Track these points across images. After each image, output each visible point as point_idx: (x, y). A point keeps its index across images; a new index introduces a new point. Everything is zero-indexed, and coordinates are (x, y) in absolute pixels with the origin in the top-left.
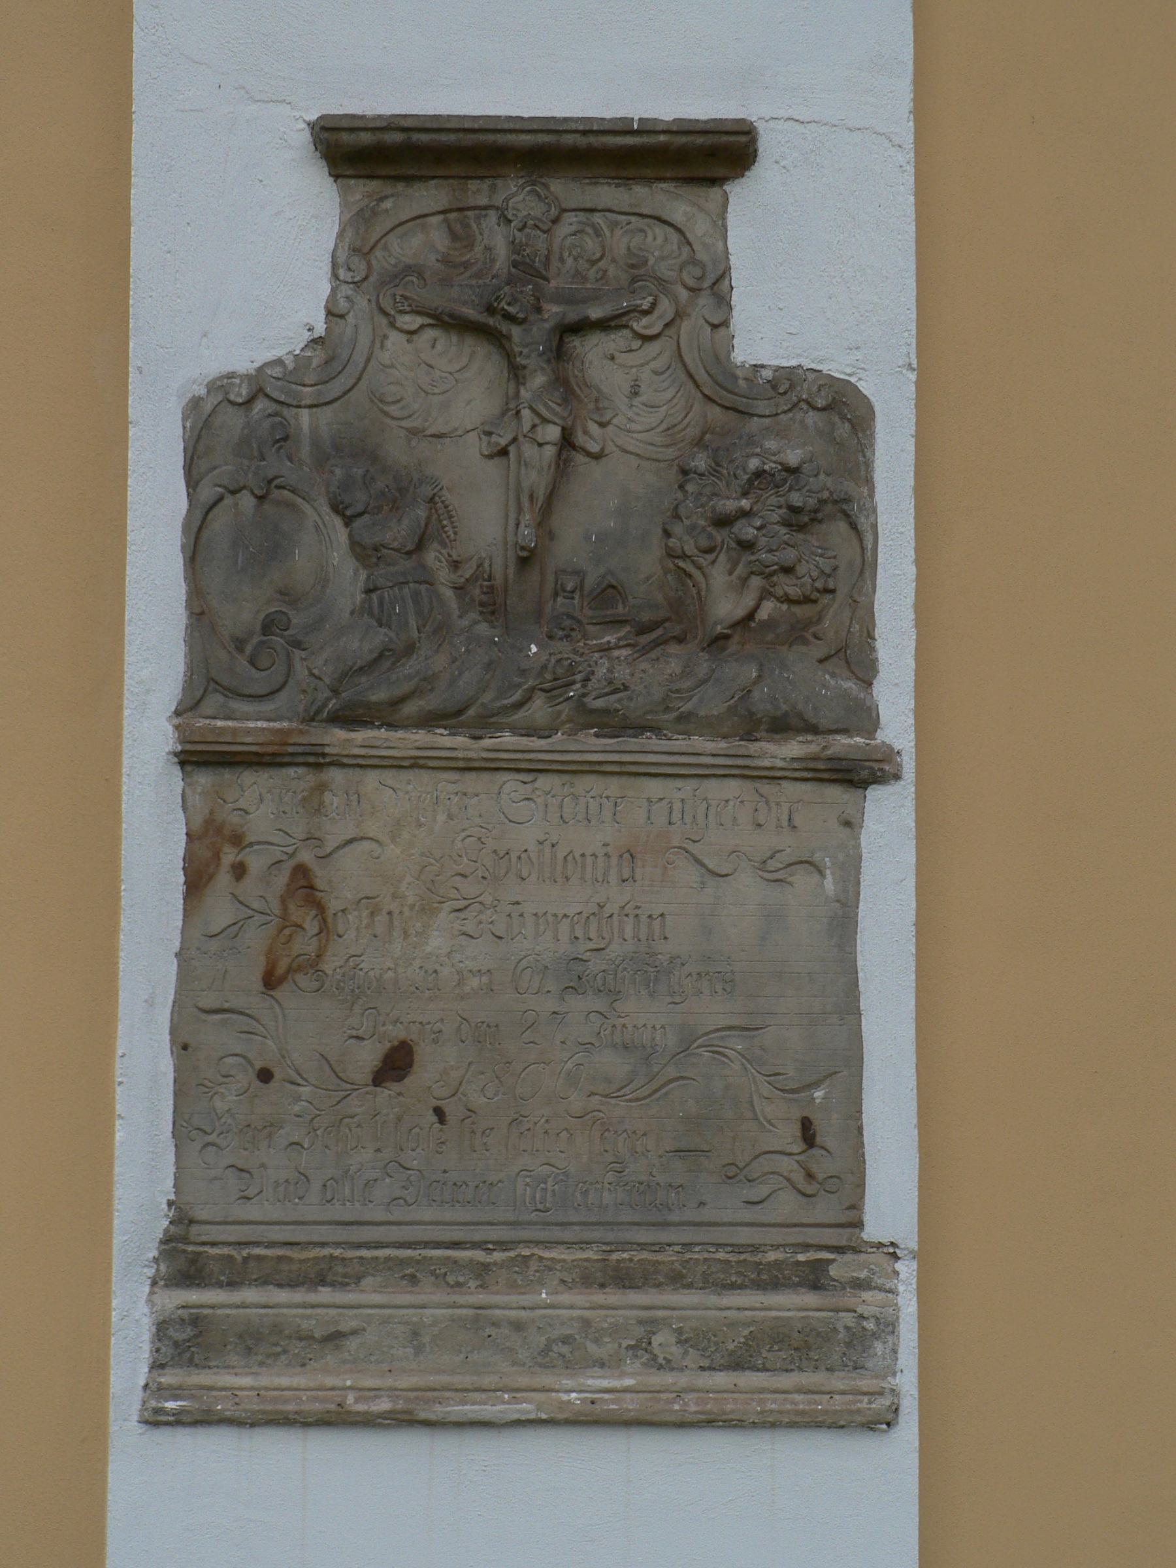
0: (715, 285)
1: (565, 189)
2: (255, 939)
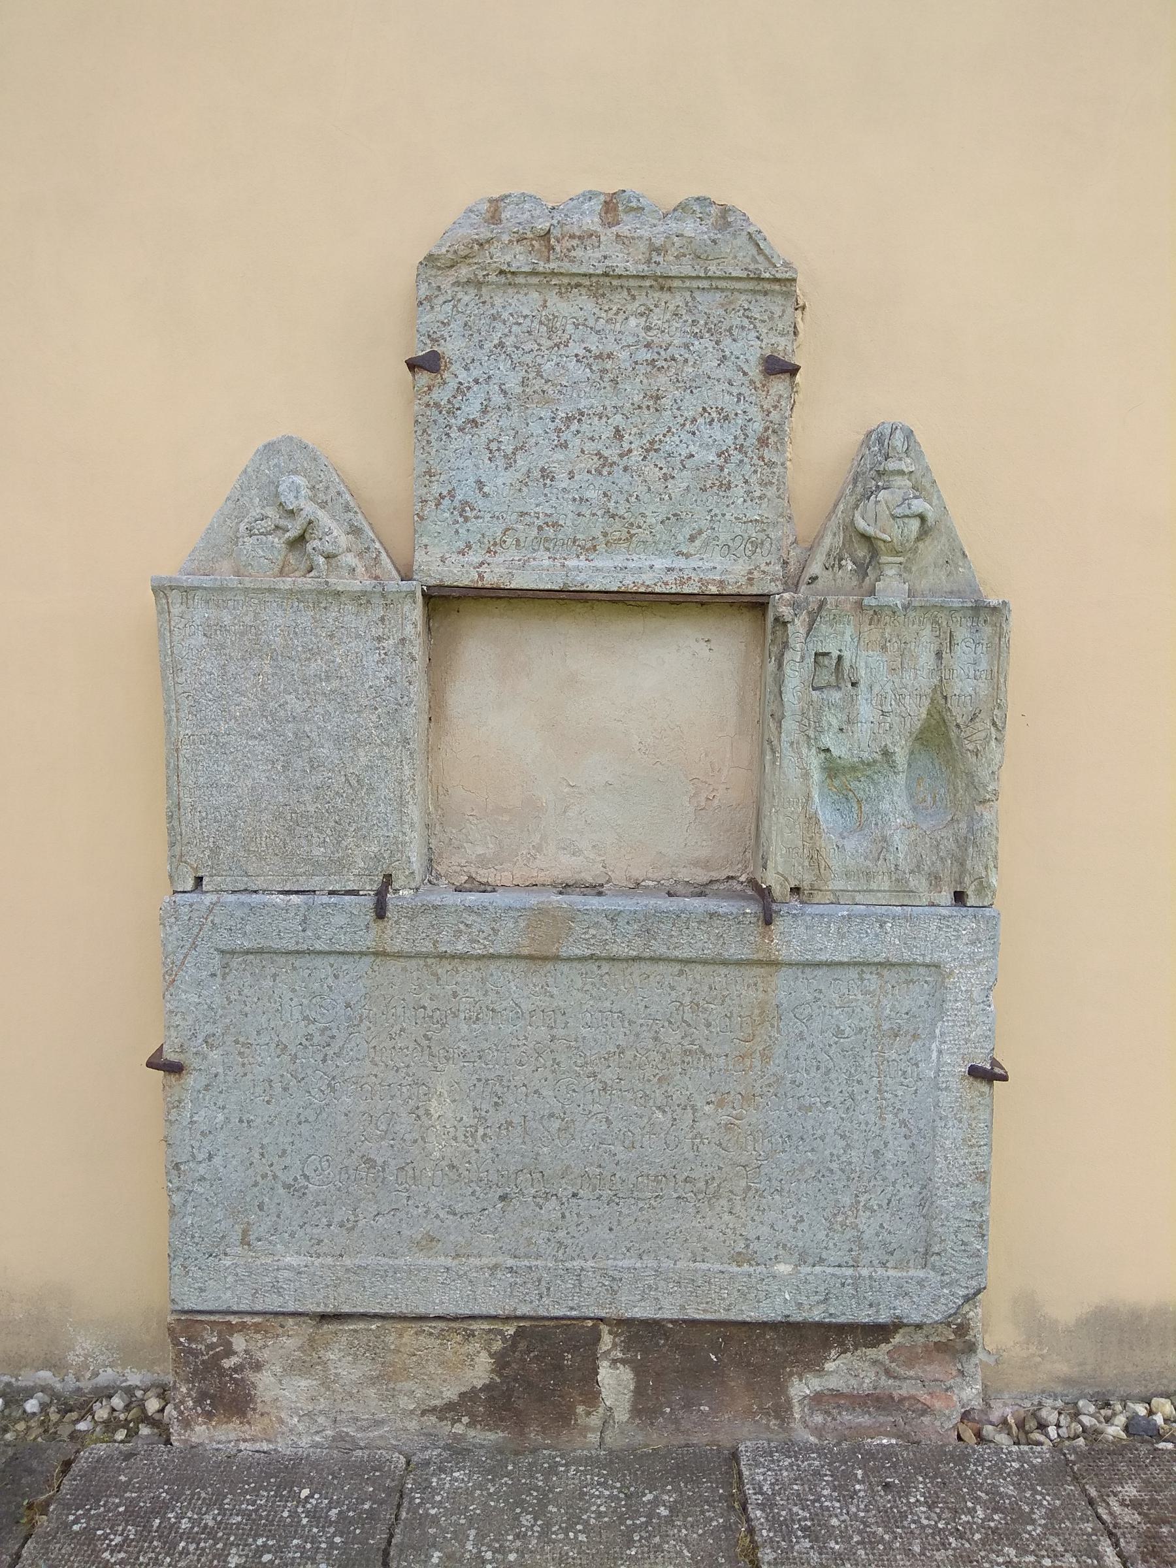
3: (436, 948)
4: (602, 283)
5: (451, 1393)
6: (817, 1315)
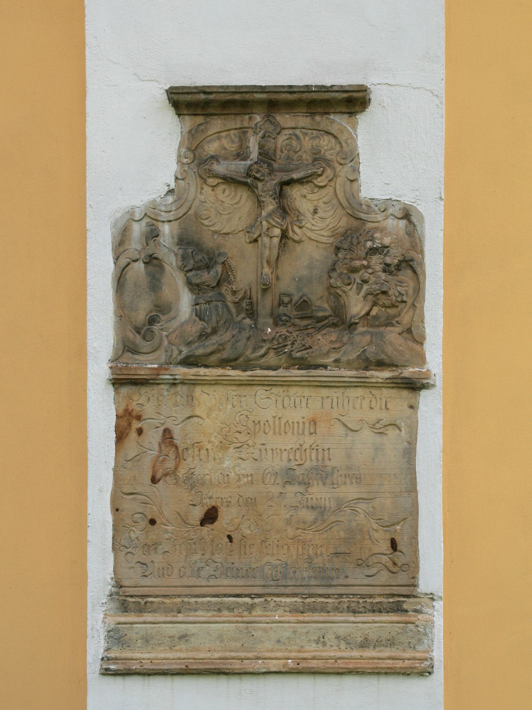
0: (350, 157)
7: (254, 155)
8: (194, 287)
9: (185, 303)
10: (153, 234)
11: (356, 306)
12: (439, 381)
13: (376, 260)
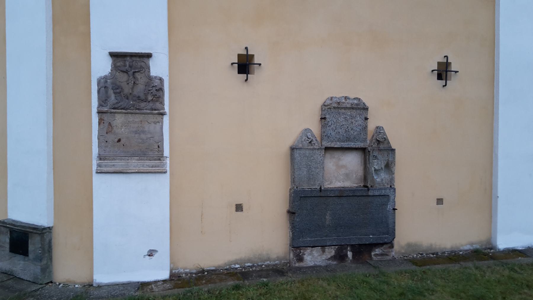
0: (149, 68)
1: (134, 59)
2: (105, 130)
3: (472, 246)
4: (345, 108)
5: (329, 257)
6: (375, 242)
7: (128, 66)
8: (115, 93)
9: (113, 97)
10: (106, 82)
11: (150, 98)
12: (168, 113)
13: (154, 88)
